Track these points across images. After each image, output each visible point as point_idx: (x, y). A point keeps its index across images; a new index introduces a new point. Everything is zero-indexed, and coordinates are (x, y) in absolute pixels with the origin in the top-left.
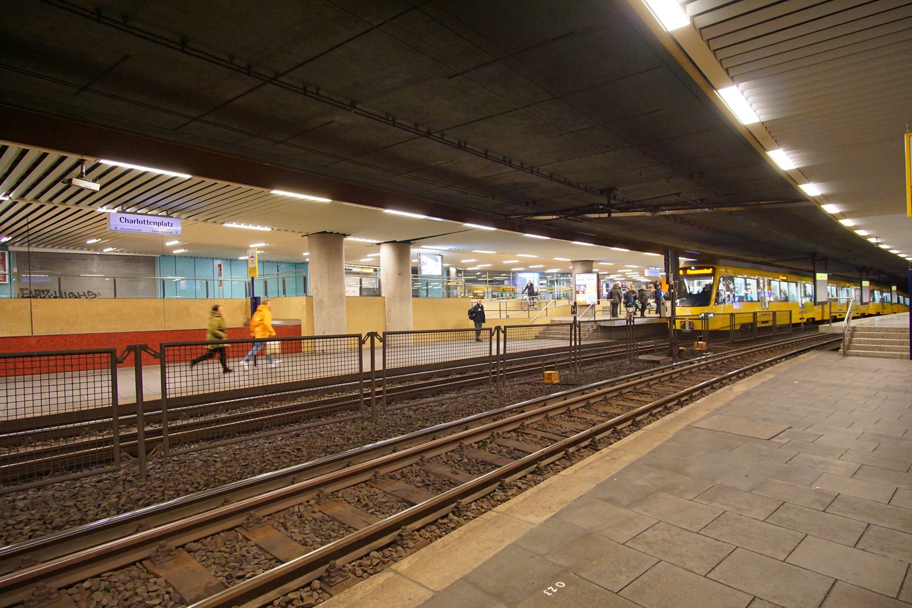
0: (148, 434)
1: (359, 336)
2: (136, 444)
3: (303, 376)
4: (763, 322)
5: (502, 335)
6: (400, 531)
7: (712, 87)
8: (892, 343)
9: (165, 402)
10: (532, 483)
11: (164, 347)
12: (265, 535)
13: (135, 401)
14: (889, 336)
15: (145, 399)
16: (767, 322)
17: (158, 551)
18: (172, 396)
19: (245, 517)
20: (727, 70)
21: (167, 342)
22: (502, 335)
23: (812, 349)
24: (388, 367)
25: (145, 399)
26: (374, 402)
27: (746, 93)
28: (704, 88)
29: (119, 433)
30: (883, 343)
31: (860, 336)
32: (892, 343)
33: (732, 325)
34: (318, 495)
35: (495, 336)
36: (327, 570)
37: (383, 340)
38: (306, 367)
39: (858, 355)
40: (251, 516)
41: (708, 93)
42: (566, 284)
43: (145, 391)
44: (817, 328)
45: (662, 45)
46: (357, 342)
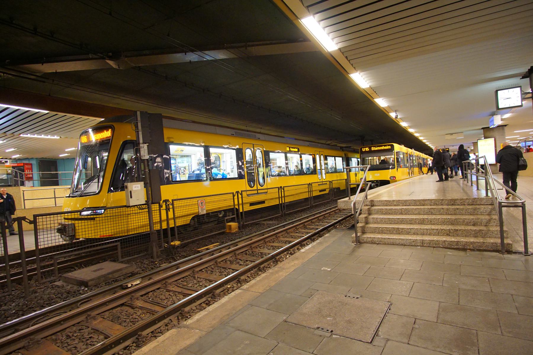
0: (29, 271)
1: (233, 193)
2: (22, 278)
3: (90, 235)
4: (252, 204)
5: (240, 196)
6: (137, 336)
7: (297, 18)
8: (411, 222)
9: (38, 251)
10: (204, 305)
11: (35, 216)
12: (98, 323)
13: (19, 251)
14: (407, 212)
15: (9, 253)
16: (325, 190)
17: (29, 343)
18: (42, 247)
19: (84, 317)
20: (352, 65)
21: (175, 198)
22: (240, 196)
23: (327, 229)
24: (41, 246)
25: (9, 253)
26: (26, 279)
27: (364, 77)
28: (344, 73)
29: (10, 271)
30: (402, 222)
31: (381, 212)
32: (411, 222)
33: (310, 191)
34: (87, 318)
35: (236, 197)
36: (137, 338)
37: (241, 194)
38: (120, 224)
39: (373, 242)
40: (132, 296)
41: (295, 22)
42: (290, 166)
43: (26, 245)
44: (337, 203)
45: (323, 53)
46: (158, 206)
